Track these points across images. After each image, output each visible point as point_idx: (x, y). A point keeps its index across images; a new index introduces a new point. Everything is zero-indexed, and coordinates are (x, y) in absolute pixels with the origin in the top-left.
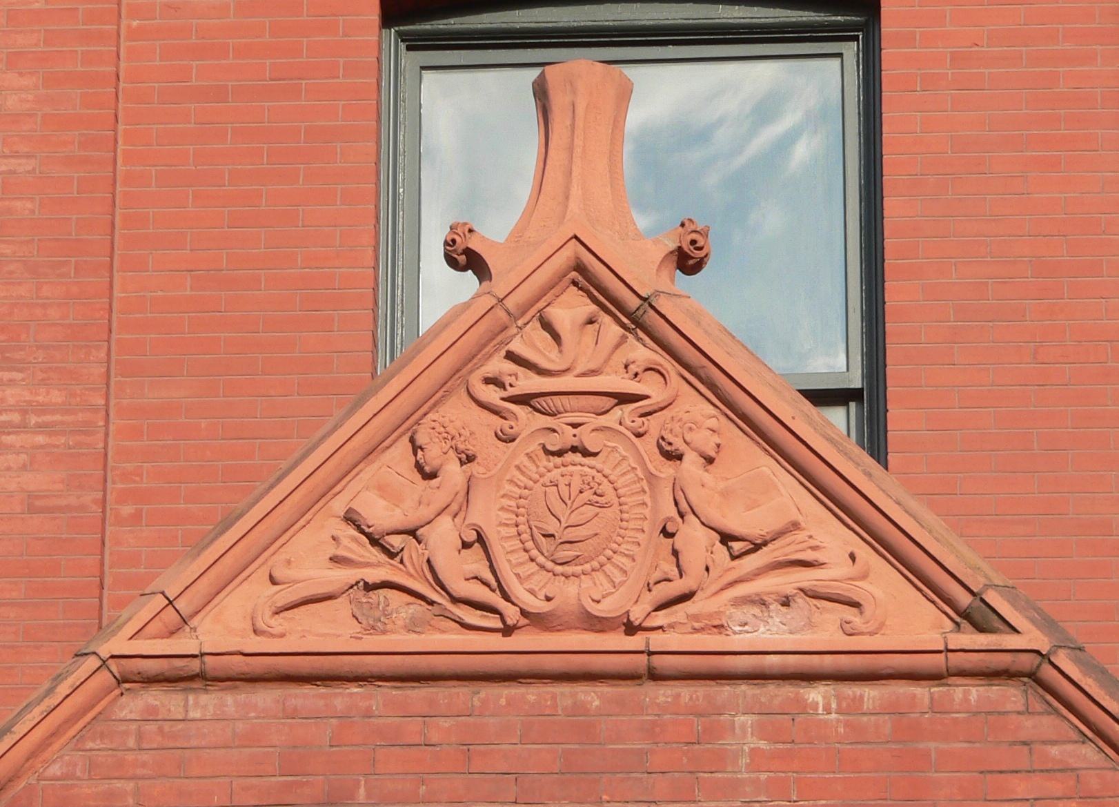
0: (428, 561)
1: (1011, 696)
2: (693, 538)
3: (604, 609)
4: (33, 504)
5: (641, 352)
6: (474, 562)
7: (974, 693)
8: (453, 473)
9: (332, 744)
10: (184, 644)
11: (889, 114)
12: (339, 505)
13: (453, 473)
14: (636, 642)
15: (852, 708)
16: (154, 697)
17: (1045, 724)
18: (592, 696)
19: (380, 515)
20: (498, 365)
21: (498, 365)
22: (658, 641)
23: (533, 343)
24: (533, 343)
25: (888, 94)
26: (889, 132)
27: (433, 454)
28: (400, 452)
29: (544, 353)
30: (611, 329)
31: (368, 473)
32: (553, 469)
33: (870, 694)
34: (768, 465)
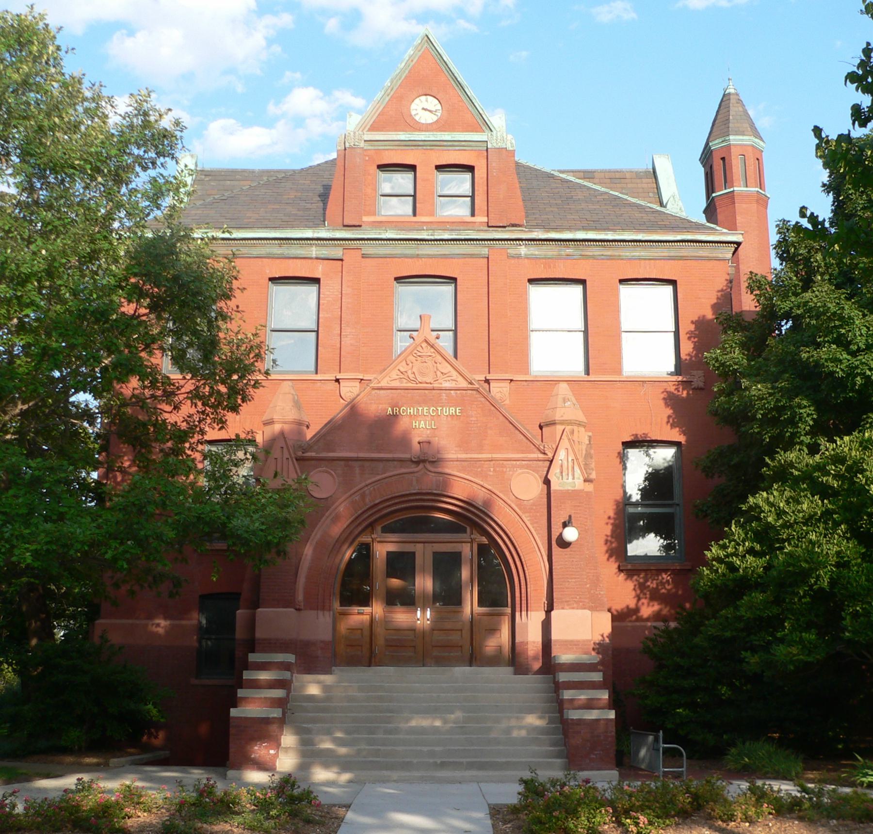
0: (360, 226)
1: (474, 392)
2: (438, 373)
3: (428, 381)
4: (351, 345)
5: (432, 350)
6: (413, 375)
7: (470, 392)
8: (411, 364)
9: (341, 262)
10: (380, 385)
11: (458, 295)
12: (397, 368)
13: (411, 364)
14: (432, 386)
15: (456, 393)
16: (376, 391)
17: (478, 396)
18: (426, 392)
19: (402, 370)
20: (416, 351)
21: (416, 351)
22: (435, 385)
23: (419, 349)
24: (419, 349)
25: (458, 293)
26: (458, 297)
27: (408, 363)
28: (404, 362)
29: (421, 351)
30: (429, 347)
31: (401, 364)
32: (422, 364)
33: (458, 392)
34: (447, 364)
